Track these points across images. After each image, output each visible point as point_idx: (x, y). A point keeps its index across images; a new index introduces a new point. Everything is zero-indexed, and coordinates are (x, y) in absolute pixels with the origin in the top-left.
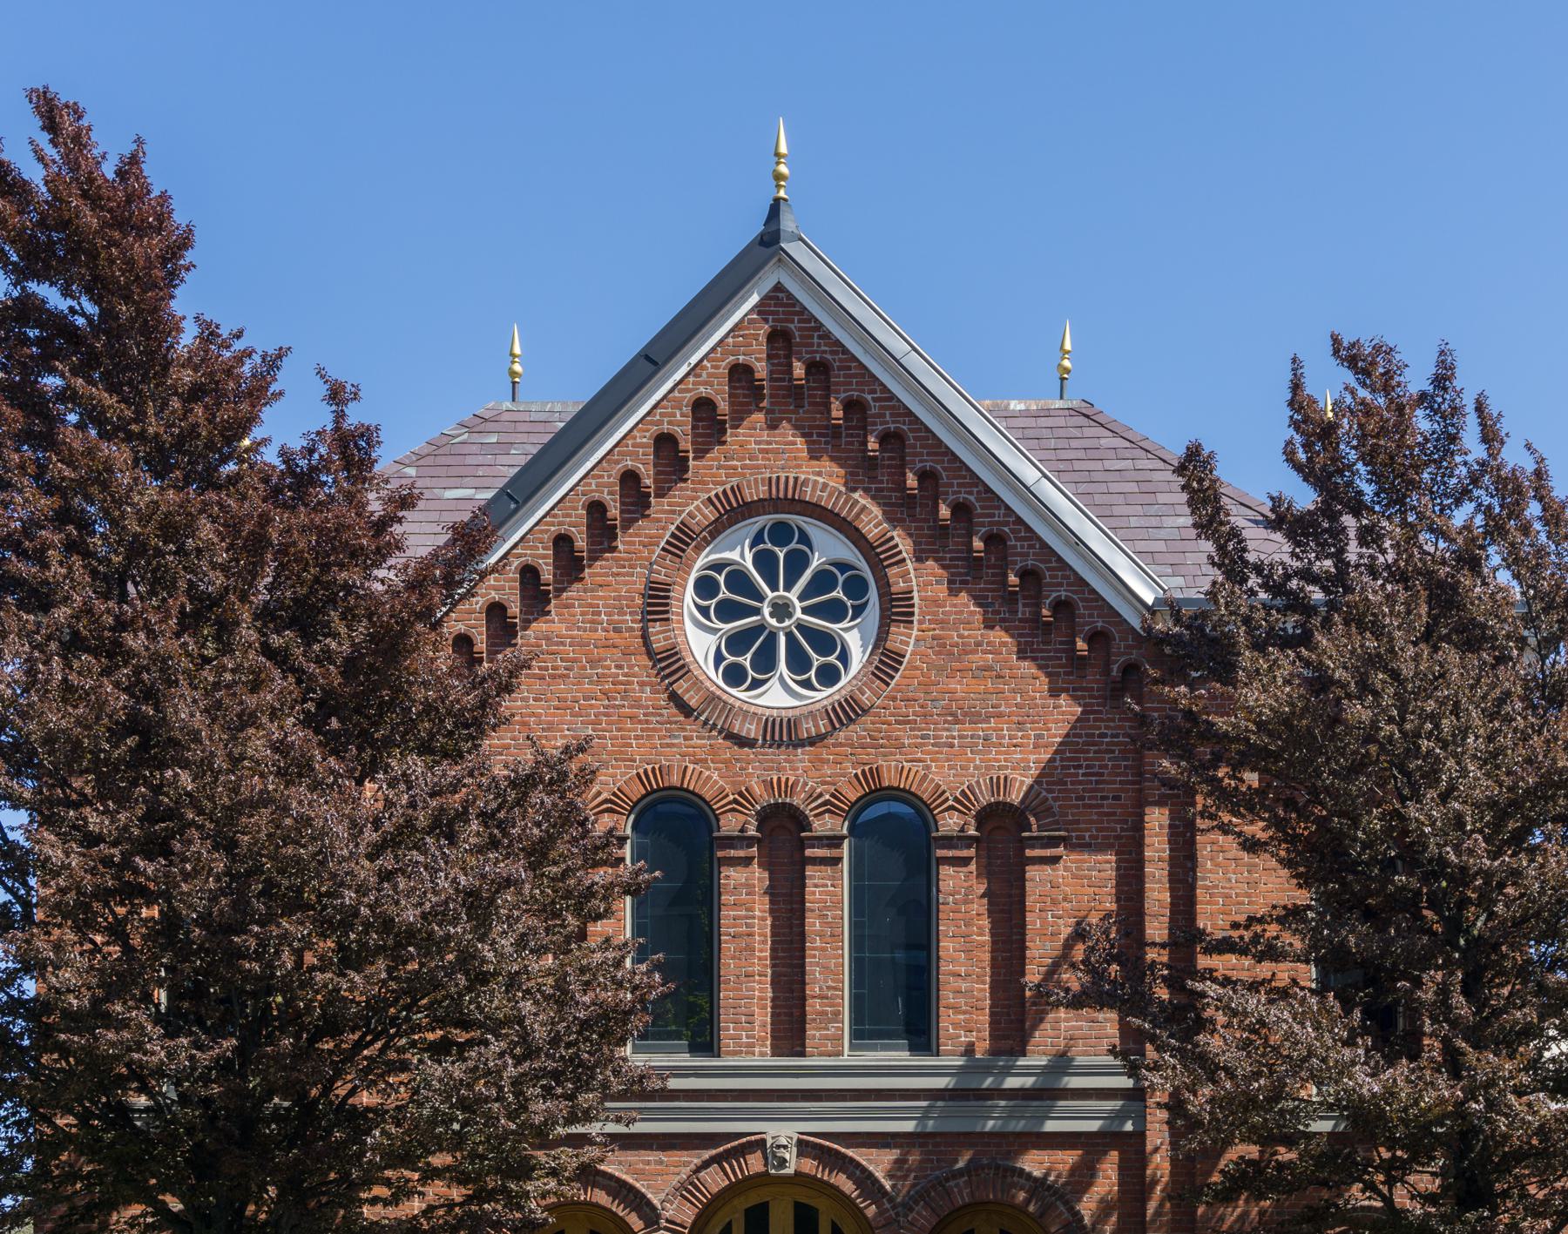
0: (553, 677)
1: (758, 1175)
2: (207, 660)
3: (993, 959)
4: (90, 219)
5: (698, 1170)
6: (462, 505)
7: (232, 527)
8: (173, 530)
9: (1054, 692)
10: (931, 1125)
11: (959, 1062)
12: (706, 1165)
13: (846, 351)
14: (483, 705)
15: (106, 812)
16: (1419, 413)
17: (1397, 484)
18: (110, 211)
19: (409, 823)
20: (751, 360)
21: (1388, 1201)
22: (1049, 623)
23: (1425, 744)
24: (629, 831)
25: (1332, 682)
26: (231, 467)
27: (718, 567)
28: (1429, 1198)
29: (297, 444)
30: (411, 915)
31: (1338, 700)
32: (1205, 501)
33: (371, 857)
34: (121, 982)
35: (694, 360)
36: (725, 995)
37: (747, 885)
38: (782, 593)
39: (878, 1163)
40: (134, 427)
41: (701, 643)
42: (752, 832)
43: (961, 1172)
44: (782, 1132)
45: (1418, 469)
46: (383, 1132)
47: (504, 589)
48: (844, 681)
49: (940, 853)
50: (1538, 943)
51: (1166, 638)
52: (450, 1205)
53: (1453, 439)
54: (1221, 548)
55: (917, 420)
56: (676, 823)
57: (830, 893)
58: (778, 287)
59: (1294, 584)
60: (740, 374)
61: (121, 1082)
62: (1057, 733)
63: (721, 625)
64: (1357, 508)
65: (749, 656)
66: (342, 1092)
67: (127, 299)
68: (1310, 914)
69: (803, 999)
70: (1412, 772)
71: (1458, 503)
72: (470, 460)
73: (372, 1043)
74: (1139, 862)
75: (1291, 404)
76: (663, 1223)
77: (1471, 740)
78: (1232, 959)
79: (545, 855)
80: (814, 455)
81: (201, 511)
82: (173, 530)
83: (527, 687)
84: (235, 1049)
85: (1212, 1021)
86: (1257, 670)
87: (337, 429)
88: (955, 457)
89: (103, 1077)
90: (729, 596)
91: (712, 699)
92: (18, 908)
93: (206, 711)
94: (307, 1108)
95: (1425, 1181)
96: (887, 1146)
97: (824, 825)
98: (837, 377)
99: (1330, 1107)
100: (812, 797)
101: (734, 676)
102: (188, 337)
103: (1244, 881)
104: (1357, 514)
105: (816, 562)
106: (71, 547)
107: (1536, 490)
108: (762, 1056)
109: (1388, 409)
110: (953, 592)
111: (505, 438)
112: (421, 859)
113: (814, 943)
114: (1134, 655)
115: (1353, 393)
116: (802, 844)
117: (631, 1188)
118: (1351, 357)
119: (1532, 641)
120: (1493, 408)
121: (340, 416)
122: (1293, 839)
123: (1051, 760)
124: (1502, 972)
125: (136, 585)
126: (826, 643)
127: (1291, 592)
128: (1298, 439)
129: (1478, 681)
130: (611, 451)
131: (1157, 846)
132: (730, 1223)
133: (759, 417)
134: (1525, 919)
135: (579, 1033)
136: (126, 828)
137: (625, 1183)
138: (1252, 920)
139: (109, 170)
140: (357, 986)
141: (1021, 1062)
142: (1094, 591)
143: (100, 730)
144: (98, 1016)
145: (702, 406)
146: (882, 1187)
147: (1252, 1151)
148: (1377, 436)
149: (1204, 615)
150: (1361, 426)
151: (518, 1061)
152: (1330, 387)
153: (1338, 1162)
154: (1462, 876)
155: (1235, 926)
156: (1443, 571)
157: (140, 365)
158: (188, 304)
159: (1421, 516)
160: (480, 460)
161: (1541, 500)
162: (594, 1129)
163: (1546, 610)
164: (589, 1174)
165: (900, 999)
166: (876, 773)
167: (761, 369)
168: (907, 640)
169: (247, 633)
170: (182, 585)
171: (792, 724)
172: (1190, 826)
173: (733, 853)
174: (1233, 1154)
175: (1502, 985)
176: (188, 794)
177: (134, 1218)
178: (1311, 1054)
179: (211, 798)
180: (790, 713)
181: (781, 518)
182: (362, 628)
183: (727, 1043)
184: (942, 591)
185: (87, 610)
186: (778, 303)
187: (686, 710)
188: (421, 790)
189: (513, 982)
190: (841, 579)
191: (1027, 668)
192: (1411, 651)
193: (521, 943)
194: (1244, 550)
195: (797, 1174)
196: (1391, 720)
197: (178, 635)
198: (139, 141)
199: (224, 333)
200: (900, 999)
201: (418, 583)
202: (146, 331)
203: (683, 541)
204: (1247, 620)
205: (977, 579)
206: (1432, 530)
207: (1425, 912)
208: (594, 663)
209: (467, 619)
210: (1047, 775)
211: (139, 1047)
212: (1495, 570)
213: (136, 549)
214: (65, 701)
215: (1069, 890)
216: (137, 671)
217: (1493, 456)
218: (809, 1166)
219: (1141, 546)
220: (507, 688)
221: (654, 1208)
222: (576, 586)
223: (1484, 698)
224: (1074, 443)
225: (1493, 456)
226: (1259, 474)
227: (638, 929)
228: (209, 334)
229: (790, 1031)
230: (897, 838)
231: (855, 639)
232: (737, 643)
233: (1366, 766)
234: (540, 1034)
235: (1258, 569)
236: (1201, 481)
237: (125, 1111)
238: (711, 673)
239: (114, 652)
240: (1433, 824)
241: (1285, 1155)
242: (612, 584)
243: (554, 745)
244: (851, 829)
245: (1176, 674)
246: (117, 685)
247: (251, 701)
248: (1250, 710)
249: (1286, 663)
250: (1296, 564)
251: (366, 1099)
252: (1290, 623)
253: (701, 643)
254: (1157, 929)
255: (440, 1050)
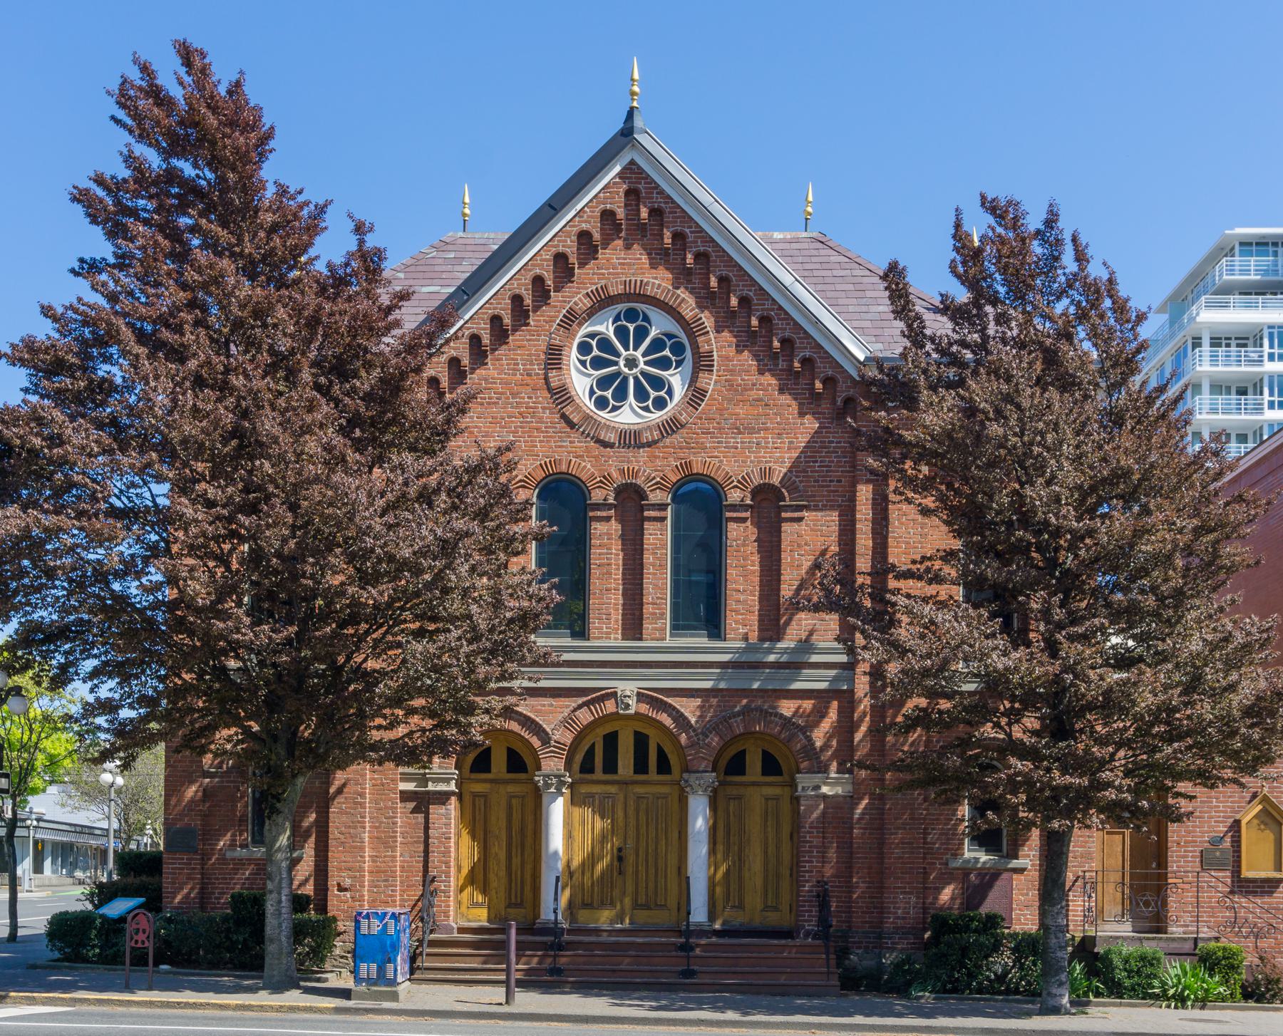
0: (489, 403)
1: (612, 714)
2: (281, 394)
3: (761, 581)
4: (212, 121)
5: (575, 710)
6: (432, 296)
7: (298, 310)
8: (260, 313)
9: (802, 414)
10: (722, 685)
11: (741, 644)
12: (580, 707)
13: (673, 202)
14: (448, 421)
15: (219, 486)
16: (1036, 243)
17: (1020, 288)
18: (225, 115)
19: (404, 495)
20: (614, 207)
21: (1009, 735)
22: (798, 372)
23: (1036, 449)
24: (535, 500)
25: (977, 410)
26: (295, 273)
27: (592, 335)
28: (1034, 733)
29: (338, 260)
30: (407, 553)
31: (982, 423)
32: (900, 297)
33: (381, 516)
34: (225, 591)
35: (579, 207)
36: (593, 602)
37: (608, 534)
38: (631, 352)
39: (690, 709)
40: (236, 249)
41: (580, 382)
42: (611, 500)
43: (738, 714)
44: (628, 688)
45: (1033, 277)
46: (386, 685)
47: (460, 349)
48: (670, 406)
49: (728, 514)
50: (1104, 574)
51: (873, 382)
52: (423, 730)
53: (1057, 259)
54: (910, 326)
55: (718, 245)
56: (563, 493)
57: (659, 539)
58: (632, 162)
59: (954, 348)
60: (607, 216)
61: (224, 652)
62: (802, 441)
63: (592, 372)
64: (995, 301)
65: (610, 391)
66: (359, 660)
67: (234, 170)
68: (961, 555)
69: (642, 604)
70: (1028, 466)
71: (1059, 299)
72: (437, 268)
73: (375, 631)
74: (853, 522)
75: (954, 237)
76: (553, 743)
77: (1065, 447)
78: (911, 582)
79: (486, 515)
80: (653, 266)
81: (278, 301)
82: (260, 313)
83: (474, 410)
84: (297, 634)
85: (900, 622)
86: (931, 404)
87: (360, 250)
88: (741, 268)
89: (212, 649)
90: (600, 354)
91: (587, 418)
92: (162, 544)
93: (280, 424)
94: (338, 670)
95: (1031, 722)
96: (693, 696)
97: (656, 497)
98: (668, 218)
99: (976, 676)
100: (649, 479)
101: (601, 403)
102: (270, 191)
103: (919, 533)
104: (994, 306)
105: (654, 332)
106: (197, 323)
107: (1109, 291)
108: (616, 640)
109: (1015, 240)
110: (739, 352)
111: (459, 255)
112: (411, 517)
113: (649, 570)
114: (852, 392)
115: (993, 229)
116: (642, 509)
117: (533, 721)
118: (991, 206)
119: (1103, 385)
120: (1083, 240)
121: (361, 242)
122: (952, 510)
123: (799, 457)
124: (1083, 592)
125: (237, 346)
126: (658, 383)
127: (953, 354)
128: (958, 258)
129: (1071, 411)
130: (526, 264)
131: (864, 511)
132: (593, 744)
133: (619, 243)
134: (1097, 560)
135: (507, 625)
136: (231, 497)
137: (529, 718)
138: (924, 558)
139: (222, 89)
140: (372, 595)
141: (779, 645)
142: (826, 352)
143: (216, 436)
144: (214, 611)
145: (584, 236)
146: (689, 722)
147: (923, 702)
148: (1008, 257)
149: (898, 368)
150: (998, 251)
151: (470, 642)
152: (978, 226)
153: (979, 710)
154: (1057, 533)
155: (914, 562)
156: (1048, 342)
157: (239, 211)
158: (271, 172)
159: (1035, 307)
160: (444, 268)
161: (1111, 297)
162: (515, 684)
163: (1113, 366)
164: (508, 712)
165: (702, 605)
166: (689, 465)
167: (621, 213)
168: (709, 382)
169: (306, 375)
170: (265, 347)
171: (637, 434)
172: (885, 498)
173: (599, 514)
174: (910, 704)
175: (1081, 600)
176: (269, 475)
177: (230, 736)
178: (963, 642)
179: (283, 478)
180: (636, 427)
181: (631, 307)
182: (376, 373)
183: (594, 632)
184: (732, 352)
185: (208, 363)
186: (632, 170)
187: (571, 425)
188: (411, 474)
189: (465, 593)
190: (668, 344)
191: (786, 399)
192: (1029, 391)
193: (473, 569)
194: (924, 327)
195: (636, 713)
196: (1015, 434)
197: (263, 378)
198: (242, 73)
199: (292, 190)
200: (702, 605)
201: (411, 348)
202: (245, 190)
203: (571, 320)
204: (925, 372)
205: (754, 344)
206: (1042, 316)
207: (1034, 555)
208: (514, 395)
209: (437, 368)
210: (795, 467)
211: (238, 631)
212: (1081, 341)
213: (238, 324)
214: (194, 418)
215: (809, 536)
216: (239, 398)
217: (1082, 269)
218: (644, 708)
219: (856, 324)
220: (463, 411)
221: (547, 734)
222: (504, 347)
223: (1074, 421)
224: (814, 259)
225: (1082, 269)
226: (933, 280)
227: (540, 563)
228: (282, 191)
229: (633, 625)
230: (701, 502)
231: (677, 380)
232: (604, 383)
233: (999, 462)
234: (483, 626)
235: (932, 340)
236: (897, 284)
237: (224, 669)
238: (587, 401)
239: (224, 388)
240: (1041, 500)
241: (945, 705)
242: (526, 346)
243: (491, 446)
244: (673, 500)
245: (878, 404)
246: (226, 408)
247: (309, 419)
248: (925, 427)
249: (950, 398)
250: (956, 337)
251: (371, 664)
252: (951, 373)
253: (580, 382)
254: (863, 563)
255: (419, 634)
